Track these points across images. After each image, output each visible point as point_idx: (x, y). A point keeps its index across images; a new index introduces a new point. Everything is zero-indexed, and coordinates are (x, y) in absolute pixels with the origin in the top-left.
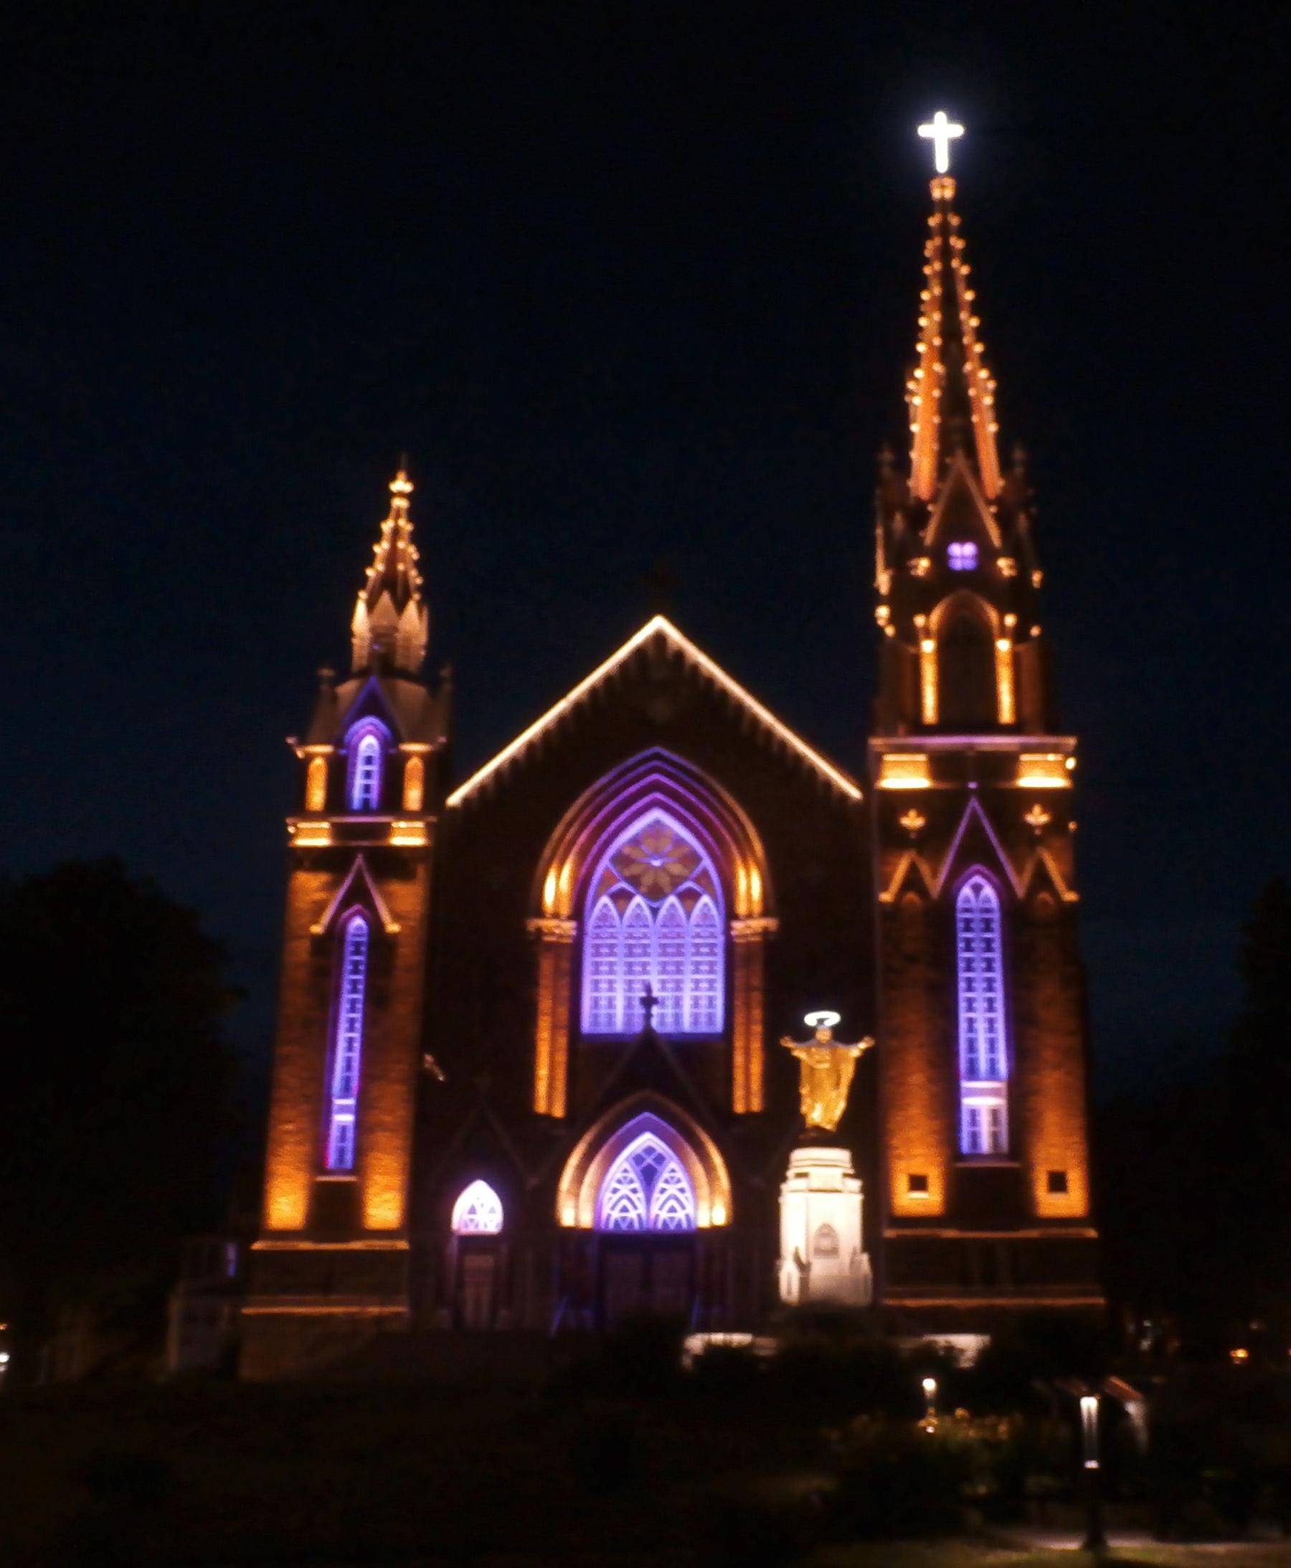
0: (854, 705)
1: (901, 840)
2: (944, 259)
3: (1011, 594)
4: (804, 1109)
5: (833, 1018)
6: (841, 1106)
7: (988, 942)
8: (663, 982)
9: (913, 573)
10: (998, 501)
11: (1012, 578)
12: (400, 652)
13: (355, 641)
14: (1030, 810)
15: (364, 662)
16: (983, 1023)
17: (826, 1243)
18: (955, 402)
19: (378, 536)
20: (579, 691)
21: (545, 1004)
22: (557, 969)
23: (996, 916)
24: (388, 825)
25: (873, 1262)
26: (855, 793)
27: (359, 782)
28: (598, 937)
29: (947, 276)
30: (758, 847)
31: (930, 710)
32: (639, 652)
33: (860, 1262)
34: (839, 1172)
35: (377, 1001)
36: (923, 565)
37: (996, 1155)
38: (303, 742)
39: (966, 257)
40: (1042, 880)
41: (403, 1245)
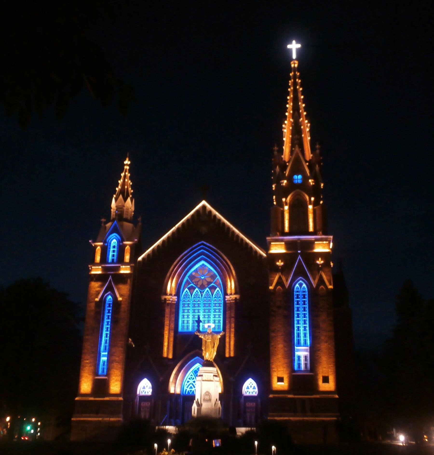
2: (295, 86)
3: (314, 191)
6: (215, 353)
7: (304, 302)
8: (204, 315)
10: (310, 162)
12: (125, 213)
13: (112, 210)
15: (114, 217)
16: (302, 329)
17: (207, 397)
18: (297, 130)
19: (120, 178)
21: (167, 322)
24: (120, 266)
26: (264, 255)
27: (111, 254)
28: (184, 301)
29: (295, 91)
31: (287, 229)
32: (198, 211)
33: (218, 404)
34: (212, 374)
35: (115, 322)
37: (306, 371)
38: (95, 241)
41: (121, 399)
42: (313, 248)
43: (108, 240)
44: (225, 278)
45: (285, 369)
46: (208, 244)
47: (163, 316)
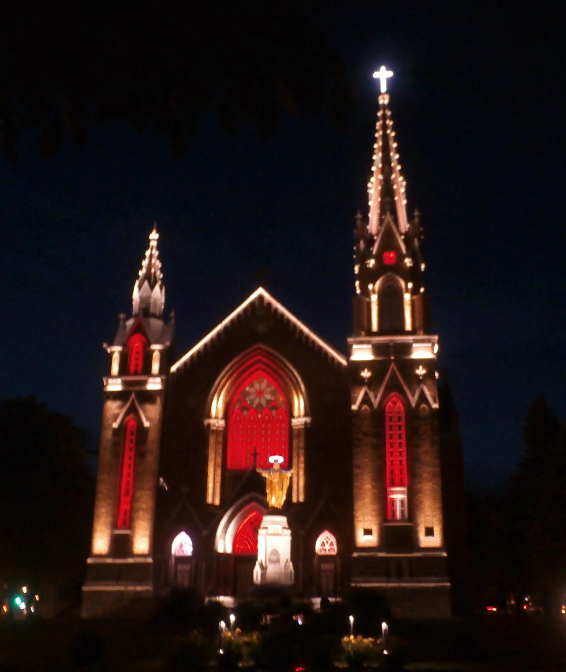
0: (343, 323)
1: (361, 382)
2: (384, 129)
3: (412, 275)
4: (268, 499)
5: (281, 459)
9: (368, 266)
10: (406, 234)
11: (411, 267)
14: (418, 368)
17: (274, 558)
18: (387, 191)
19: (144, 257)
20: (226, 321)
25: (295, 566)
26: (344, 362)
29: (385, 137)
30: (303, 387)
31: (375, 327)
32: (252, 304)
33: (289, 567)
36: (372, 263)
39: (394, 128)
40: (423, 398)
41: (150, 560)
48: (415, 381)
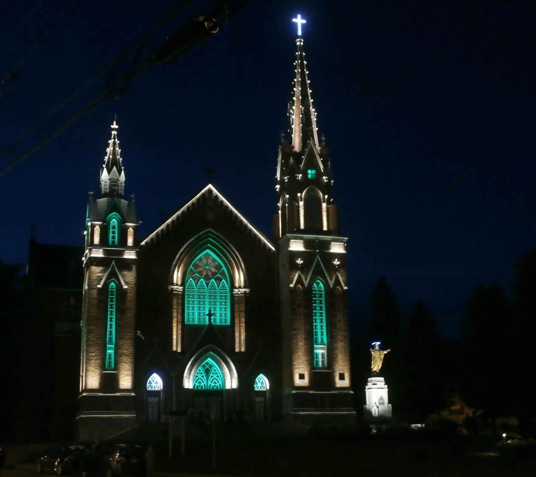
1: (294, 267)
3: (326, 189)
7: (321, 301)
22: (178, 303)
23: (323, 293)
29: (302, 74)
32: (203, 195)
35: (121, 312)
37: (323, 368)
41: (133, 394)
42: (329, 248)
43: (107, 219)
44: (233, 269)
45: (306, 367)
46: (216, 233)
47: (171, 307)
48: (332, 269)
